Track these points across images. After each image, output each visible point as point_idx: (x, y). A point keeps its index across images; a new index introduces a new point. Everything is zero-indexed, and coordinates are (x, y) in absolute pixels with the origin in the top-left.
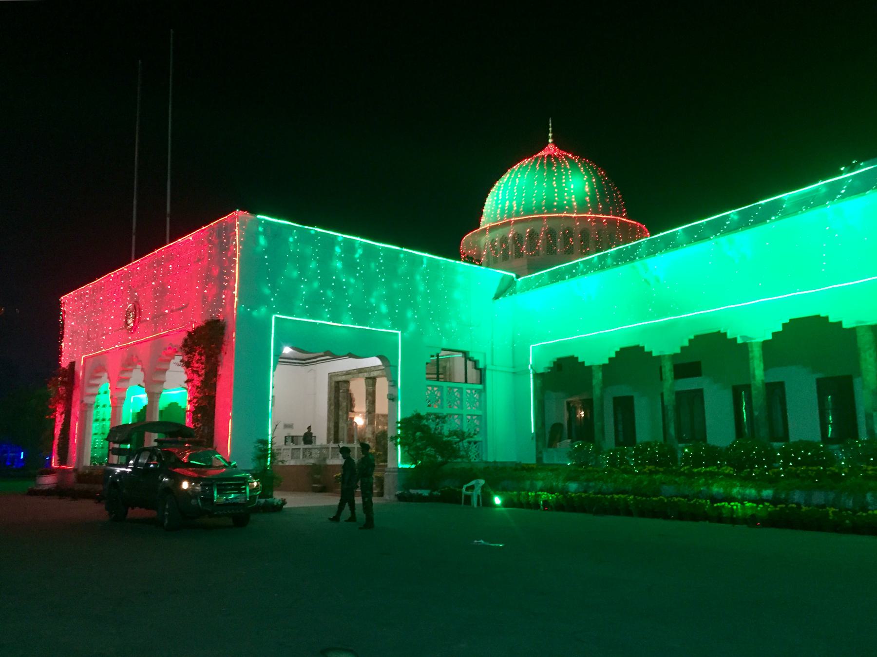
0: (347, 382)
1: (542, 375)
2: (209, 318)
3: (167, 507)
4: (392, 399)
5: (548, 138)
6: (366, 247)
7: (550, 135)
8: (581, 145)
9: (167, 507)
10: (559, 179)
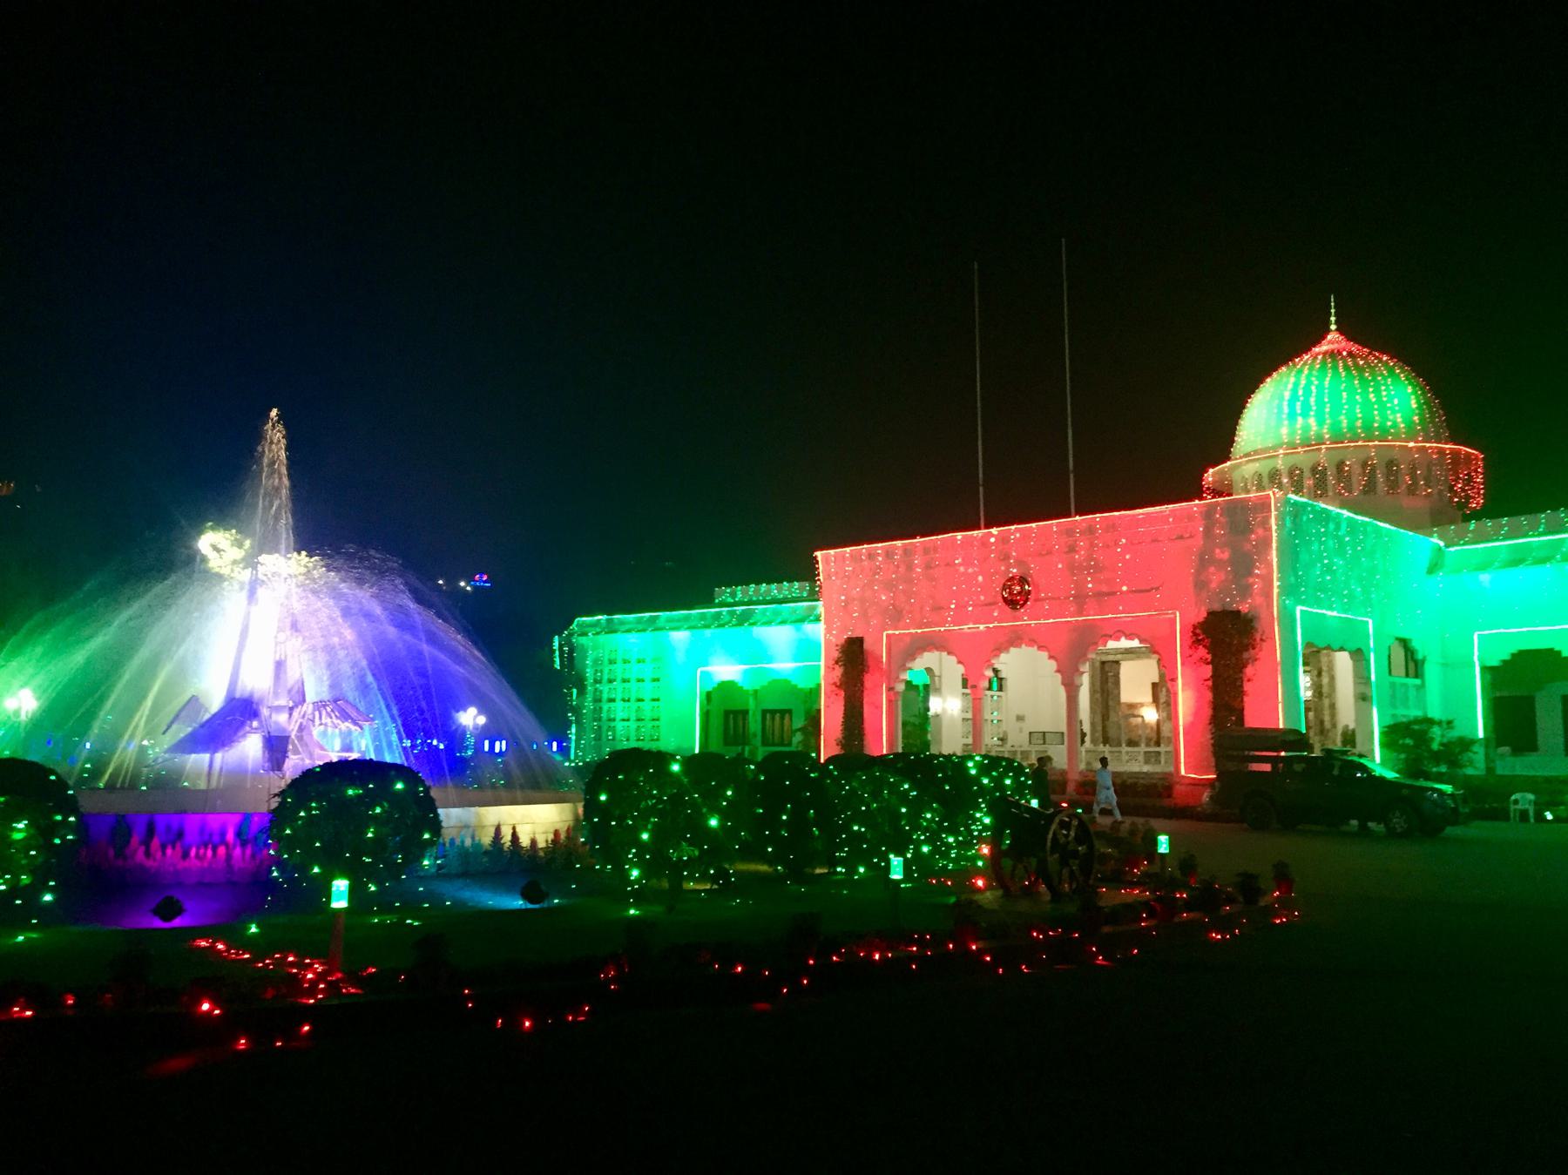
0: (1117, 663)
1: (1492, 669)
2: (1217, 607)
3: (59, 818)
4: (1363, 698)
5: (1328, 323)
6: (1350, 522)
7: (1333, 319)
8: (1382, 334)
9: (59, 818)
10: (1377, 391)
